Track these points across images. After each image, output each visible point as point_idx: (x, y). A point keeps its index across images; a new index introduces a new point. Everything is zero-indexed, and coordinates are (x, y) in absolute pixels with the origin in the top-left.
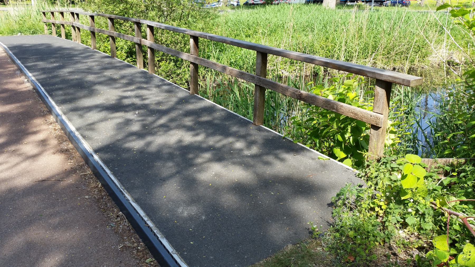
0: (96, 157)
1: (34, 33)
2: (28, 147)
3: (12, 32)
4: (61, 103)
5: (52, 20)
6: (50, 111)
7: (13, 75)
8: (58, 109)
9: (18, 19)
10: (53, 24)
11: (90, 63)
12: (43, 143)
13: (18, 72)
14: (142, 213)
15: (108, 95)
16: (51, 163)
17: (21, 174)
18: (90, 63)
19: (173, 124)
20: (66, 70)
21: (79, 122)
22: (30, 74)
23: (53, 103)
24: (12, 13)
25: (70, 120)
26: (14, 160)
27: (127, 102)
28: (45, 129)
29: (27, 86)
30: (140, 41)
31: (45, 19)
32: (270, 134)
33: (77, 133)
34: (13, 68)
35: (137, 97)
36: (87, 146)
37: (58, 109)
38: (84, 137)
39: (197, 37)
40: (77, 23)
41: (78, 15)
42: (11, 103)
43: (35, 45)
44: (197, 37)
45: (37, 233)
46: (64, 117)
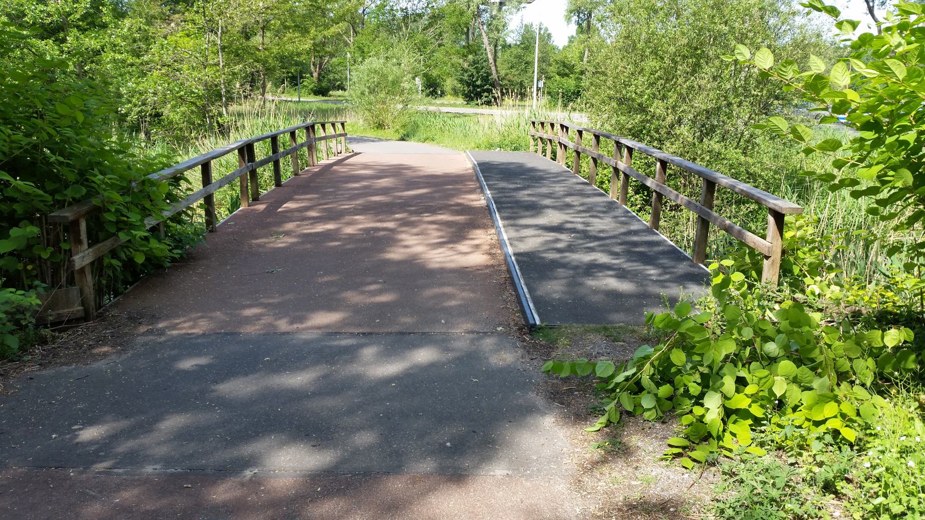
0: (513, 258)
1: (516, 149)
2: (463, 247)
3: (491, 146)
4: (503, 218)
5: (541, 133)
6: (493, 225)
7: (472, 191)
8: (500, 223)
9: (503, 129)
10: (550, 141)
11: (559, 189)
12: (477, 246)
13: (479, 190)
14: (526, 290)
15: (553, 217)
16: (478, 259)
17: (451, 261)
18: (559, 189)
19: (600, 249)
20: (526, 192)
21: (513, 234)
22: (488, 192)
23: (499, 218)
24: (498, 120)
25: (506, 232)
26: (450, 253)
27: (569, 226)
28: (482, 237)
29: (483, 202)
30: (616, 164)
31: (532, 130)
32: (701, 271)
33: (507, 242)
34: (472, 185)
35: (583, 223)
36: (510, 250)
37: (500, 223)
38: (511, 244)
39: (666, 163)
40: (565, 140)
41: (567, 128)
42: (462, 215)
43: (503, 164)
44: (666, 163)
45: (448, 290)
46: (502, 230)
